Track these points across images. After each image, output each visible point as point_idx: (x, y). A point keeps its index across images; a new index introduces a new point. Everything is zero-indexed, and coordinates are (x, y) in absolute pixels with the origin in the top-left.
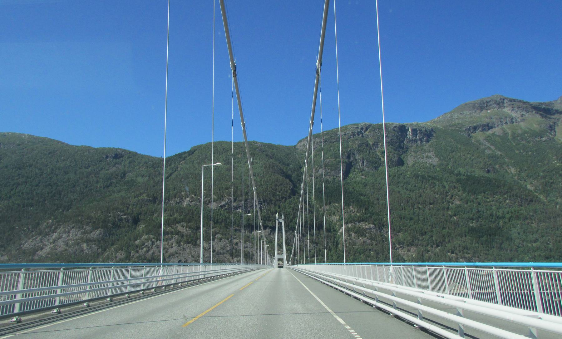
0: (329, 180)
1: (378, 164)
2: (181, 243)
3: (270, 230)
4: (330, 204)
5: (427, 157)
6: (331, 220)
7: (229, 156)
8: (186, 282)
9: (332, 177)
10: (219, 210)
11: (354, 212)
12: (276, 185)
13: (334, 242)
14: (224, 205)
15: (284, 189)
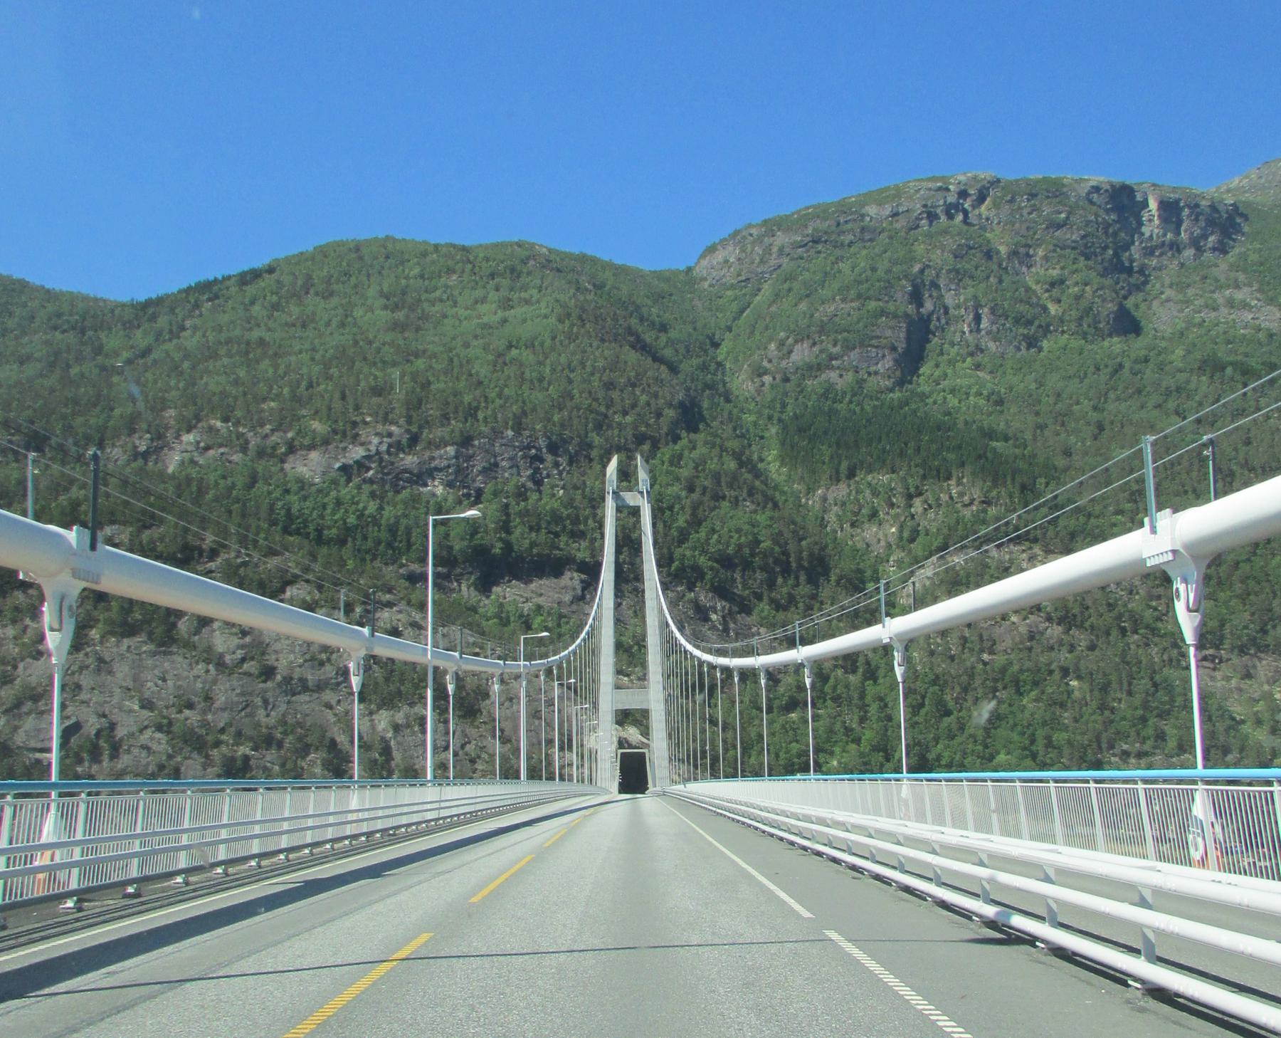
0: (839, 387)
1: (1040, 326)
2: (94, 631)
3: (582, 581)
4: (851, 474)
5: (1231, 303)
6: (861, 545)
7: (407, 278)
9: (850, 374)
10: (334, 482)
11: (971, 503)
12: (610, 386)
14: (357, 462)
15: (648, 404)
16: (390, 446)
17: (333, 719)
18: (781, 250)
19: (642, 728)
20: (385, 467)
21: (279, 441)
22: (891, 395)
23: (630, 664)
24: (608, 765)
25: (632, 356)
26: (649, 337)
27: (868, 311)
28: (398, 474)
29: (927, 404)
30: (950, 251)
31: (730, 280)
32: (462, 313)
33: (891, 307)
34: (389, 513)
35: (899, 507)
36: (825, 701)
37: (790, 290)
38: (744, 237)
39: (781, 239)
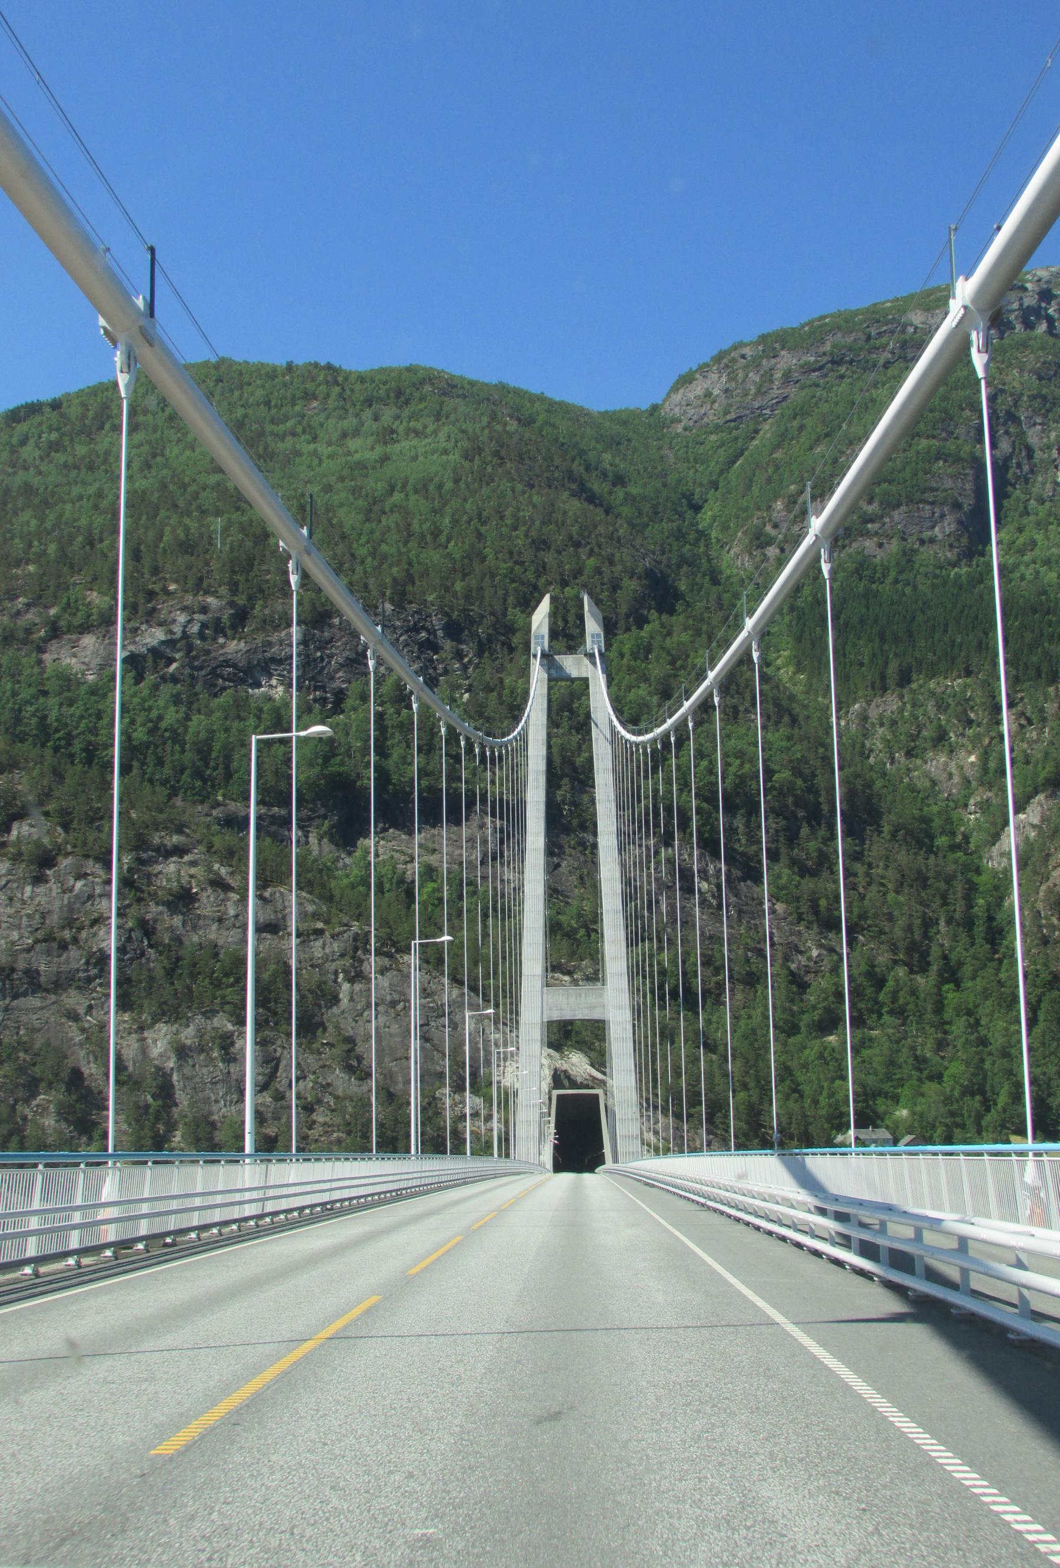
0: (877, 560)
4: (904, 679)
6: (923, 784)
8: (235, 1221)
9: (895, 542)
13: (969, 924)
14: (153, 651)
15: (598, 571)
16: (204, 626)
17: (79, 1038)
18: (787, 378)
19: (593, 1054)
20: (195, 658)
21: (37, 620)
22: (957, 569)
23: (572, 955)
24: (534, 1115)
25: (574, 506)
26: (597, 486)
27: (918, 453)
28: (215, 669)
29: (1011, 581)
30: (1030, 372)
31: (712, 419)
32: (324, 450)
33: (951, 446)
34: (198, 724)
35: (979, 725)
36: (880, 1015)
37: (801, 428)
38: (733, 361)
39: (787, 360)
